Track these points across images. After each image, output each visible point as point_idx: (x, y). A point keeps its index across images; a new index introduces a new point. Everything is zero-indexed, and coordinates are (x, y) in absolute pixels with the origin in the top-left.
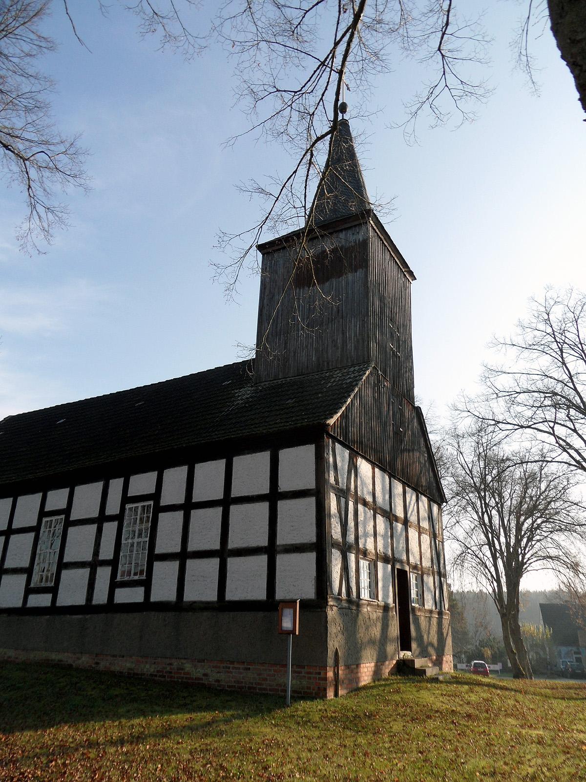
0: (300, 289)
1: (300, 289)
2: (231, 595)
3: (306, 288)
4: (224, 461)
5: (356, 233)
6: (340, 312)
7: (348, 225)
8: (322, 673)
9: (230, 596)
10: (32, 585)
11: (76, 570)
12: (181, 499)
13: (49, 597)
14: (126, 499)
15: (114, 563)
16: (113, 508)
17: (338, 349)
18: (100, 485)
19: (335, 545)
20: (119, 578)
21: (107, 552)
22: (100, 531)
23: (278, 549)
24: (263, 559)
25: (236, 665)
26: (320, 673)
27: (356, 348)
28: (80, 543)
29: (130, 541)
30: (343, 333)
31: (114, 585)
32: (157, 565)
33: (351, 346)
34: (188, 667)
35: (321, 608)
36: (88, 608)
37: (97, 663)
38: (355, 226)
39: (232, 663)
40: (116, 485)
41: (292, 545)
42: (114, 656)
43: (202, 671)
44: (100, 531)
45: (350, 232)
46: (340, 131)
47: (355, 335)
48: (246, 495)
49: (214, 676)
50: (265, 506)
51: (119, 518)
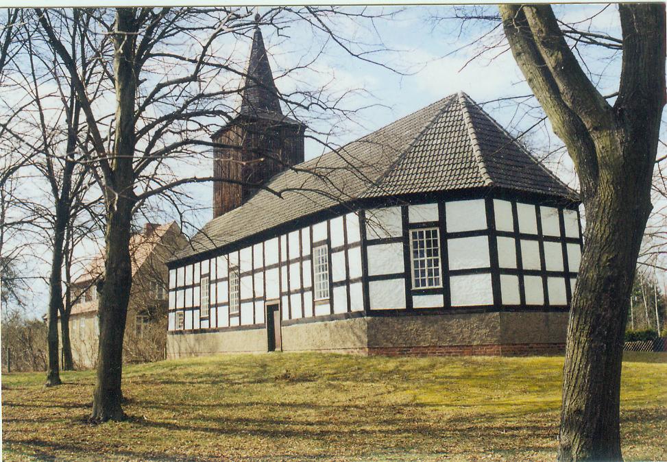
16: (306, 252)
18: (325, 223)
51: (311, 257)
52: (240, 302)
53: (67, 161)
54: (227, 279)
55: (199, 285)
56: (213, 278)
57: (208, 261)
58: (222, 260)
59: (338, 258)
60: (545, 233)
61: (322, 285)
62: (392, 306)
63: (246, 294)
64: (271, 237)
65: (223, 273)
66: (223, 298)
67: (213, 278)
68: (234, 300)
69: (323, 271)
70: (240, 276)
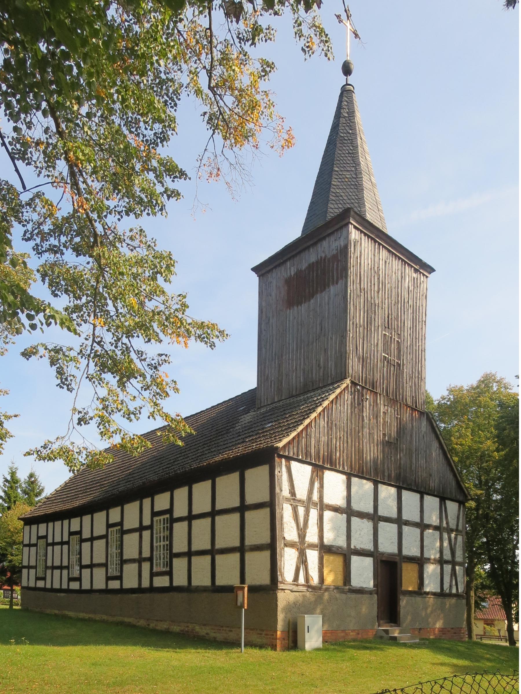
0: (290, 309)
1: (290, 309)
2: (219, 582)
3: (295, 308)
4: (210, 481)
5: (338, 238)
6: (323, 331)
7: (330, 231)
8: (275, 634)
9: (218, 583)
10: (109, 575)
11: (130, 565)
12: (185, 514)
13: (118, 582)
14: (154, 514)
15: (150, 559)
16: (147, 522)
17: (321, 368)
18: (137, 503)
19: (461, 564)
20: (155, 570)
21: (146, 554)
22: (141, 537)
23: (246, 548)
24: (237, 555)
25: (224, 628)
26: (273, 635)
27: (336, 366)
28: (131, 546)
29: (158, 544)
30: (325, 351)
31: (152, 575)
32: (175, 561)
33: (331, 364)
34: (197, 628)
35: (273, 591)
36: (139, 590)
37: (149, 625)
38: (337, 230)
39: (222, 627)
40: (147, 502)
41: (255, 545)
42: (157, 621)
43: (205, 631)
44: (141, 537)
45: (332, 238)
46: (346, 93)
47: (336, 353)
48: (225, 508)
49: (212, 635)
50: (236, 517)
51: (150, 527)
52: (123, 562)
53: (153, 123)
54: (105, 537)
55: (150, 527)
56: (50, 540)
57: (209, 483)
58: (100, 517)
59: (180, 529)
60: (405, 517)
61: (160, 555)
62: (415, 575)
63: (180, 545)
64: (100, 510)
65: (100, 529)
66: (99, 558)
67: (50, 540)
68: (114, 560)
69: (164, 541)
70: (123, 532)
